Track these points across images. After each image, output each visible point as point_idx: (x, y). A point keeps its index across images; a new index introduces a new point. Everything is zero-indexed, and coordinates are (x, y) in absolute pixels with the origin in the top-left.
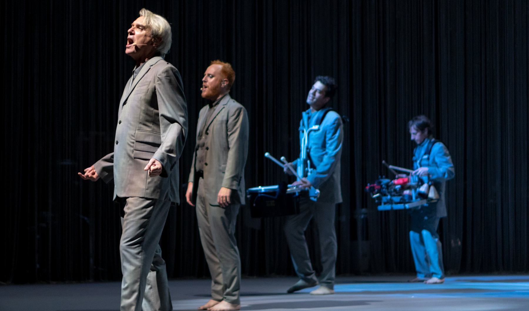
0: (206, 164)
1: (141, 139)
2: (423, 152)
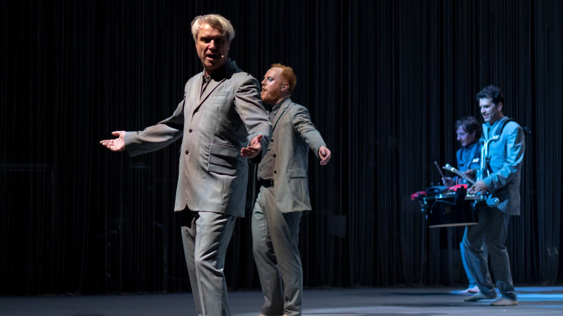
0: (275, 172)
1: (216, 153)
2: (472, 155)
